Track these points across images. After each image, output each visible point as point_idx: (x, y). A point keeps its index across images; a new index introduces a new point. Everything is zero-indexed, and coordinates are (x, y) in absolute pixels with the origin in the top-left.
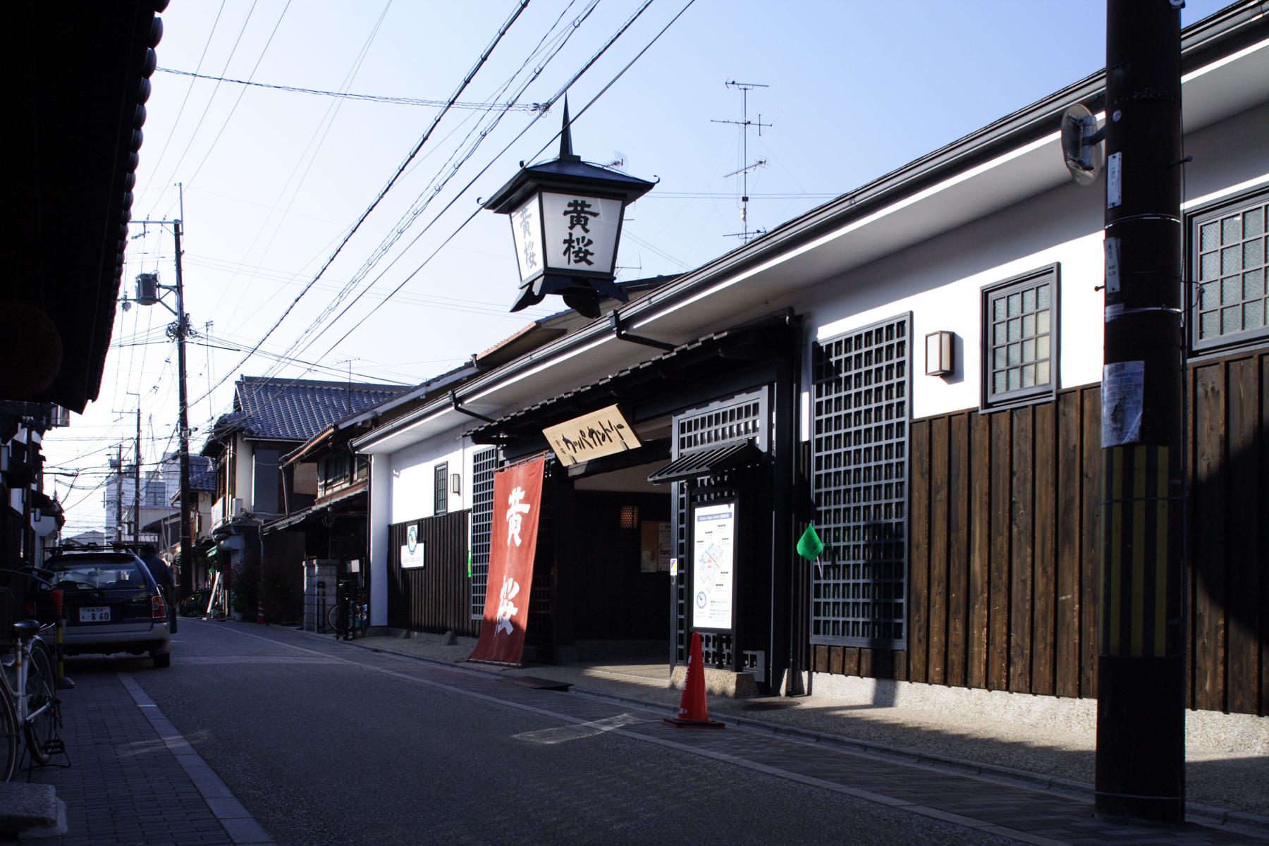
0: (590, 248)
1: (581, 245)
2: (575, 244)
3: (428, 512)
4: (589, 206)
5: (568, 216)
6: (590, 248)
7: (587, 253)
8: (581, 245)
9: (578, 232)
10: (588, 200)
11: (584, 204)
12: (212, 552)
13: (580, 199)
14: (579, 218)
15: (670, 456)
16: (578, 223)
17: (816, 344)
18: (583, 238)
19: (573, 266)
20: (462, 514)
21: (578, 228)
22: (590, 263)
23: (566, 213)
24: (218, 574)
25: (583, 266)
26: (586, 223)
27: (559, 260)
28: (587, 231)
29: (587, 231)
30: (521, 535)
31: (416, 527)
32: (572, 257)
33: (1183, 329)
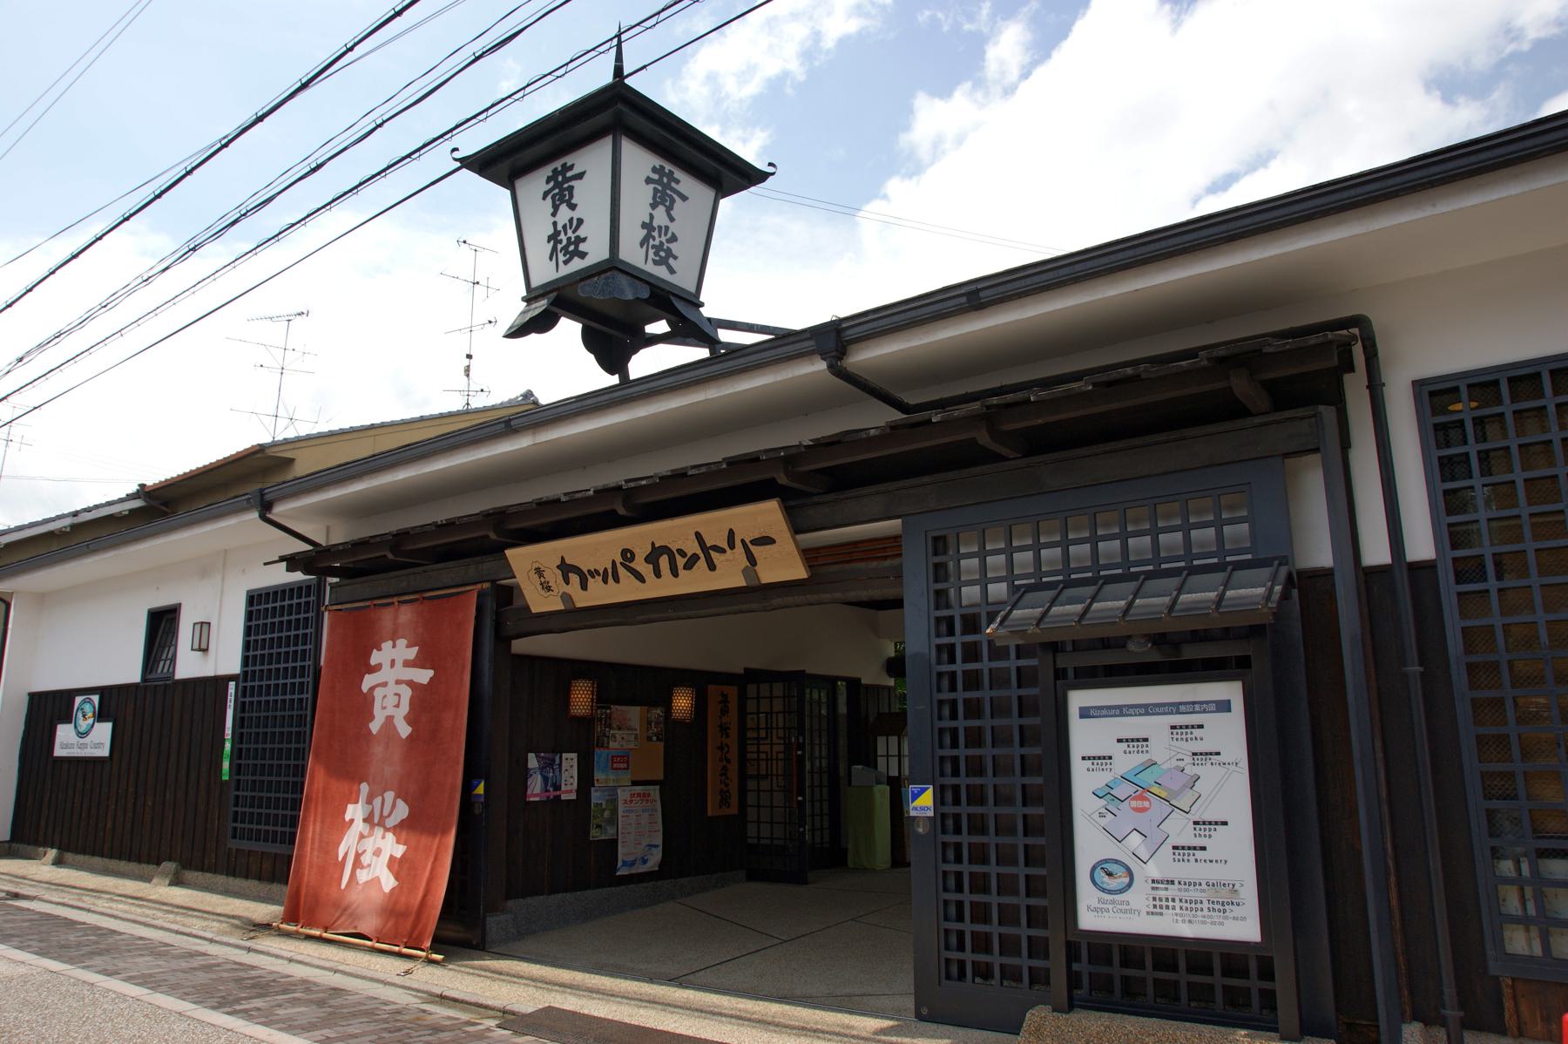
1: (570, 233)
2: (562, 237)
3: (131, 672)
4: (678, 182)
6: (581, 233)
8: (663, 239)
9: (564, 214)
10: (678, 174)
13: (558, 164)
14: (562, 190)
15: (1034, 667)
18: (667, 228)
20: (217, 684)
26: (571, 196)
27: (545, 272)
28: (672, 219)
29: (672, 219)
30: (410, 719)
31: (96, 698)
32: (561, 258)
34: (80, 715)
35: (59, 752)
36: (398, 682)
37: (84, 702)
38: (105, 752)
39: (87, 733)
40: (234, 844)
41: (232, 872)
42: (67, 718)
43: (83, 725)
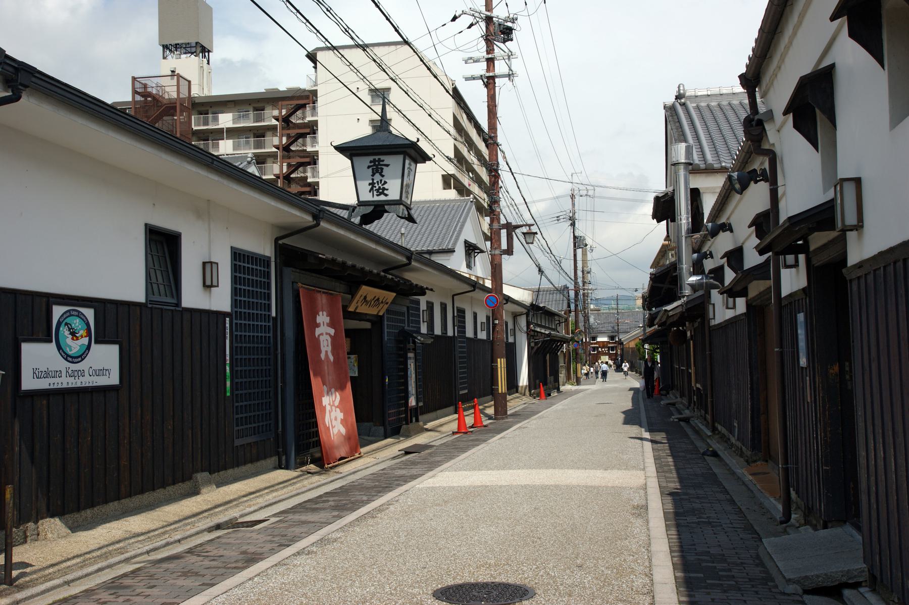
0: (386, 186)
5: (370, 169)
6: (386, 186)
7: (384, 189)
9: (377, 177)
10: (382, 158)
11: (380, 160)
12: (650, 365)
13: (377, 158)
16: (377, 172)
17: (710, 327)
19: (376, 198)
21: (377, 175)
22: (386, 195)
23: (369, 167)
24: (466, 391)
25: (382, 198)
29: (383, 176)
32: (375, 193)
33: (275, 319)
34: (64, 331)
35: (29, 383)
36: (327, 334)
37: (68, 314)
38: (113, 379)
39: (81, 357)
40: (238, 442)
41: (237, 464)
42: (45, 334)
43: (74, 347)
